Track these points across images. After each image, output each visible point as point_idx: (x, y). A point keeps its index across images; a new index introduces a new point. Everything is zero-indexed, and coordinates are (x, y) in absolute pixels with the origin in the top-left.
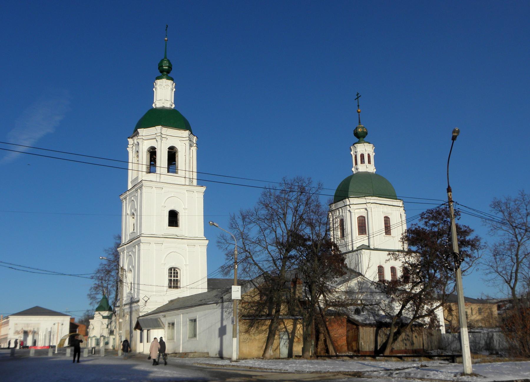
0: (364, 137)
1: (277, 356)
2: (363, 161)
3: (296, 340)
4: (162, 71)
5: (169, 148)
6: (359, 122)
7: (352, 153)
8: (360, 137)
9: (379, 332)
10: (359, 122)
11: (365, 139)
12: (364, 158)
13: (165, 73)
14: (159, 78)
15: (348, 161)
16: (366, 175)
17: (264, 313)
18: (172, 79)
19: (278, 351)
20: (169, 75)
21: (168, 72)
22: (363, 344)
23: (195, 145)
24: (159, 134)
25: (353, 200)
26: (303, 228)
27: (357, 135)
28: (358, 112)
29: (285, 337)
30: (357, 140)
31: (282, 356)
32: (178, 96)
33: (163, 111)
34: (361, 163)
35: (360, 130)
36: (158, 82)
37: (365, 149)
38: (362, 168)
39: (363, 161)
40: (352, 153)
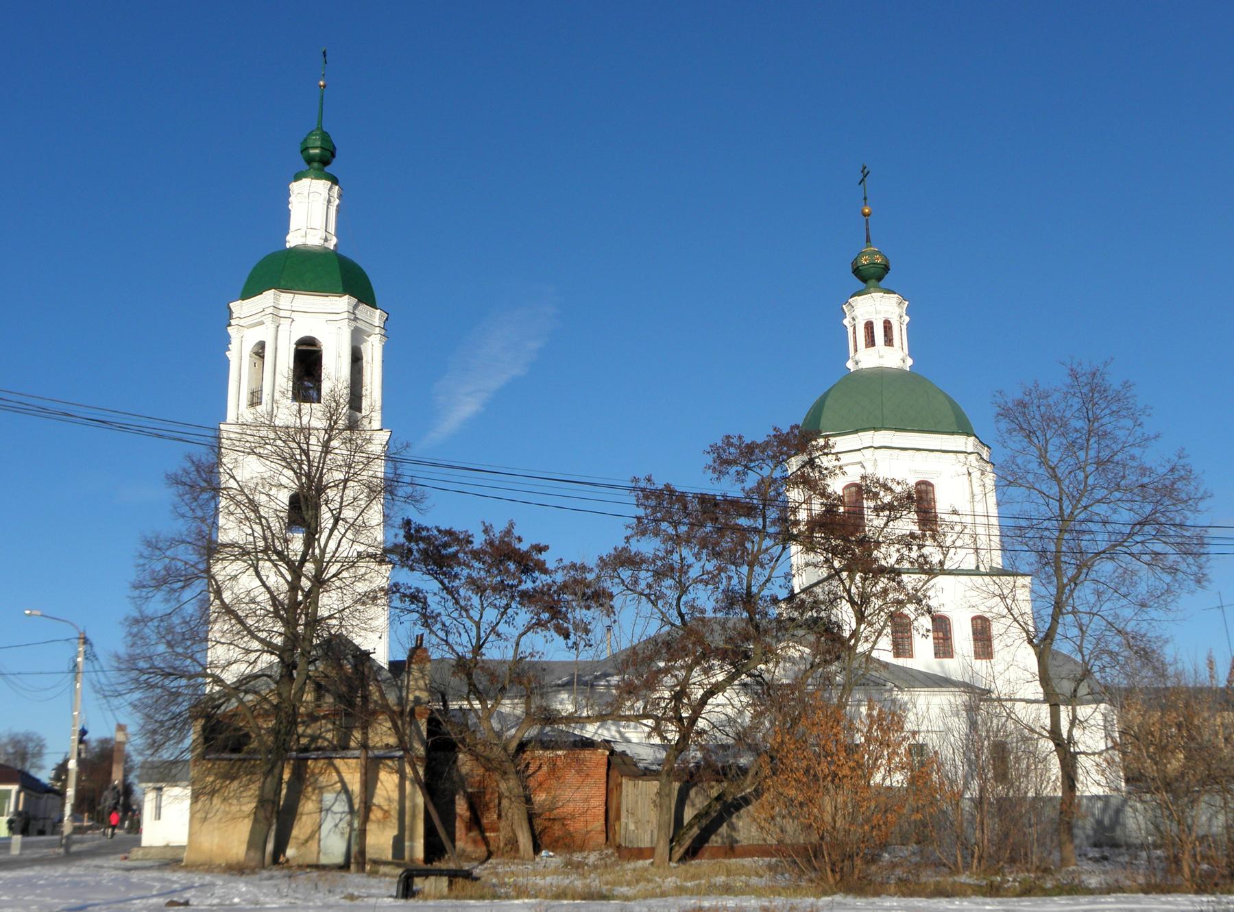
0: (879, 279)
1: (311, 859)
2: (871, 342)
3: (376, 814)
4: (310, 160)
5: (300, 343)
6: (868, 240)
7: (846, 322)
8: (870, 277)
9: (692, 793)
10: (868, 240)
11: (882, 283)
12: (878, 330)
13: (321, 163)
14: (298, 177)
15: (839, 343)
16: (881, 376)
17: (326, 744)
18: (335, 181)
19: (313, 845)
20: (327, 169)
21: (325, 161)
22: (632, 827)
23: (377, 330)
24: (271, 310)
25: (841, 443)
26: (235, 485)
27: (857, 271)
28: (865, 215)
29: (341, 807)
30: (862, 285)
31: (324, 860)
32: (345, 218)
33: (304, 256)
34: (867, 346)
35: (864, 261)
36: (295, 187)
37: (876, 307)
38: (866, 358)
39: (871, 342)
40: (846, 322)
